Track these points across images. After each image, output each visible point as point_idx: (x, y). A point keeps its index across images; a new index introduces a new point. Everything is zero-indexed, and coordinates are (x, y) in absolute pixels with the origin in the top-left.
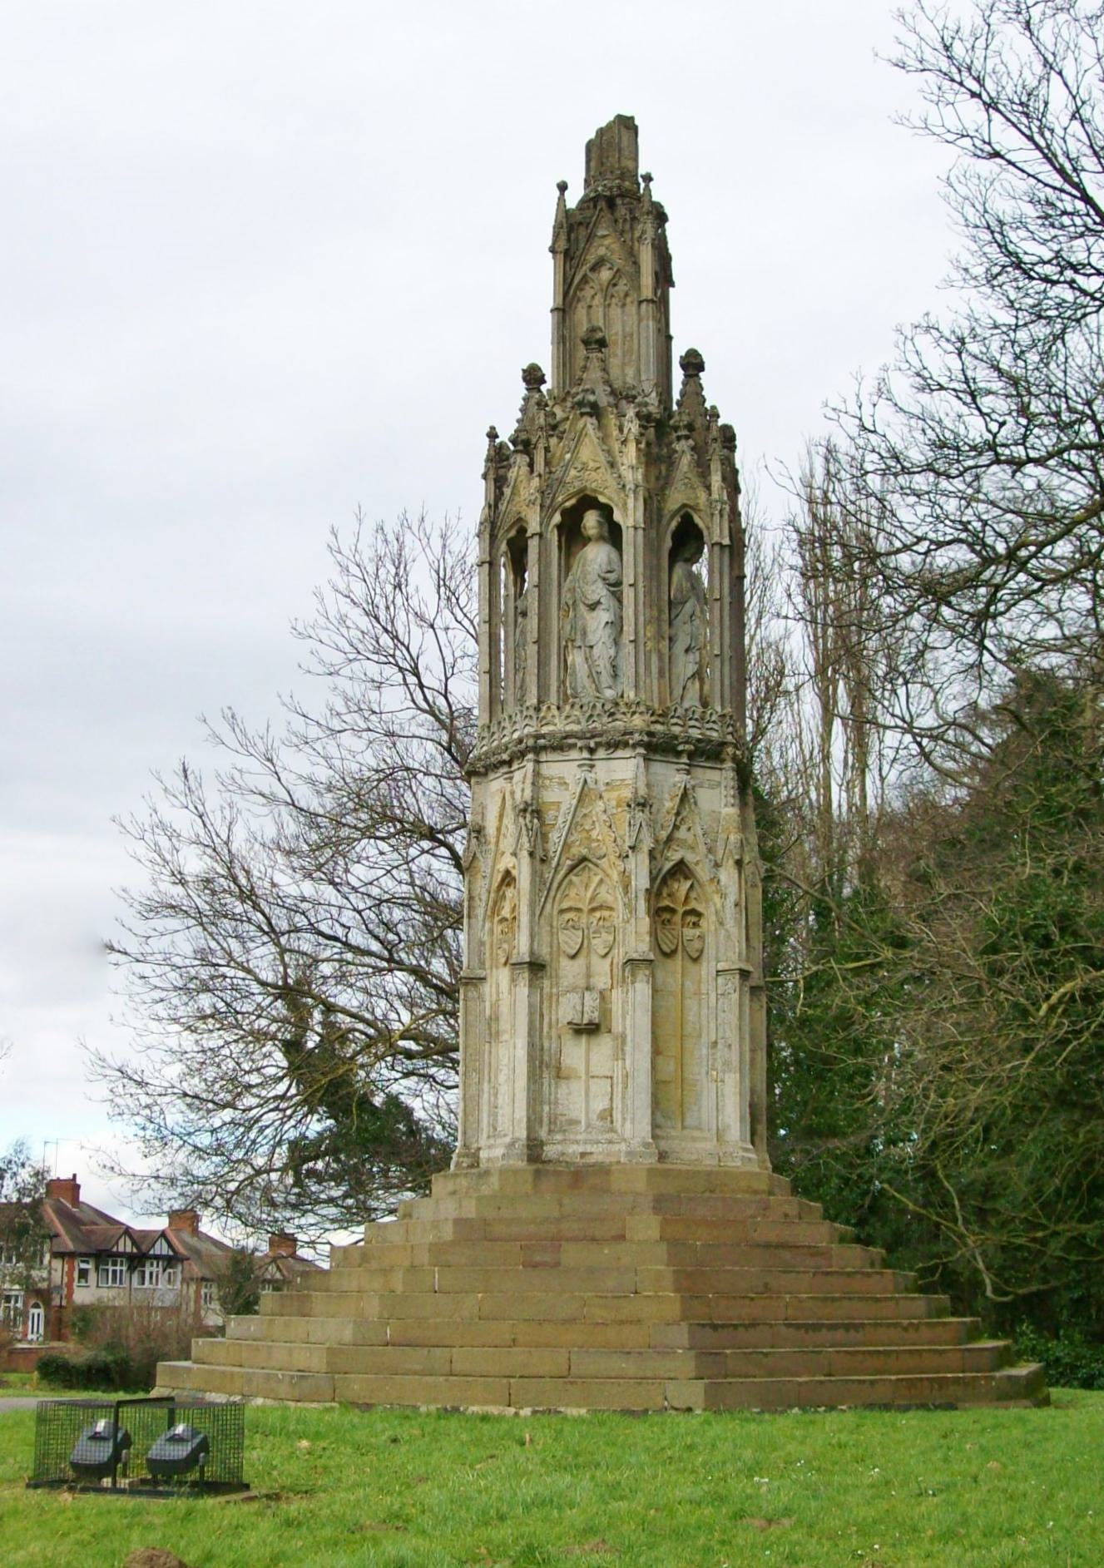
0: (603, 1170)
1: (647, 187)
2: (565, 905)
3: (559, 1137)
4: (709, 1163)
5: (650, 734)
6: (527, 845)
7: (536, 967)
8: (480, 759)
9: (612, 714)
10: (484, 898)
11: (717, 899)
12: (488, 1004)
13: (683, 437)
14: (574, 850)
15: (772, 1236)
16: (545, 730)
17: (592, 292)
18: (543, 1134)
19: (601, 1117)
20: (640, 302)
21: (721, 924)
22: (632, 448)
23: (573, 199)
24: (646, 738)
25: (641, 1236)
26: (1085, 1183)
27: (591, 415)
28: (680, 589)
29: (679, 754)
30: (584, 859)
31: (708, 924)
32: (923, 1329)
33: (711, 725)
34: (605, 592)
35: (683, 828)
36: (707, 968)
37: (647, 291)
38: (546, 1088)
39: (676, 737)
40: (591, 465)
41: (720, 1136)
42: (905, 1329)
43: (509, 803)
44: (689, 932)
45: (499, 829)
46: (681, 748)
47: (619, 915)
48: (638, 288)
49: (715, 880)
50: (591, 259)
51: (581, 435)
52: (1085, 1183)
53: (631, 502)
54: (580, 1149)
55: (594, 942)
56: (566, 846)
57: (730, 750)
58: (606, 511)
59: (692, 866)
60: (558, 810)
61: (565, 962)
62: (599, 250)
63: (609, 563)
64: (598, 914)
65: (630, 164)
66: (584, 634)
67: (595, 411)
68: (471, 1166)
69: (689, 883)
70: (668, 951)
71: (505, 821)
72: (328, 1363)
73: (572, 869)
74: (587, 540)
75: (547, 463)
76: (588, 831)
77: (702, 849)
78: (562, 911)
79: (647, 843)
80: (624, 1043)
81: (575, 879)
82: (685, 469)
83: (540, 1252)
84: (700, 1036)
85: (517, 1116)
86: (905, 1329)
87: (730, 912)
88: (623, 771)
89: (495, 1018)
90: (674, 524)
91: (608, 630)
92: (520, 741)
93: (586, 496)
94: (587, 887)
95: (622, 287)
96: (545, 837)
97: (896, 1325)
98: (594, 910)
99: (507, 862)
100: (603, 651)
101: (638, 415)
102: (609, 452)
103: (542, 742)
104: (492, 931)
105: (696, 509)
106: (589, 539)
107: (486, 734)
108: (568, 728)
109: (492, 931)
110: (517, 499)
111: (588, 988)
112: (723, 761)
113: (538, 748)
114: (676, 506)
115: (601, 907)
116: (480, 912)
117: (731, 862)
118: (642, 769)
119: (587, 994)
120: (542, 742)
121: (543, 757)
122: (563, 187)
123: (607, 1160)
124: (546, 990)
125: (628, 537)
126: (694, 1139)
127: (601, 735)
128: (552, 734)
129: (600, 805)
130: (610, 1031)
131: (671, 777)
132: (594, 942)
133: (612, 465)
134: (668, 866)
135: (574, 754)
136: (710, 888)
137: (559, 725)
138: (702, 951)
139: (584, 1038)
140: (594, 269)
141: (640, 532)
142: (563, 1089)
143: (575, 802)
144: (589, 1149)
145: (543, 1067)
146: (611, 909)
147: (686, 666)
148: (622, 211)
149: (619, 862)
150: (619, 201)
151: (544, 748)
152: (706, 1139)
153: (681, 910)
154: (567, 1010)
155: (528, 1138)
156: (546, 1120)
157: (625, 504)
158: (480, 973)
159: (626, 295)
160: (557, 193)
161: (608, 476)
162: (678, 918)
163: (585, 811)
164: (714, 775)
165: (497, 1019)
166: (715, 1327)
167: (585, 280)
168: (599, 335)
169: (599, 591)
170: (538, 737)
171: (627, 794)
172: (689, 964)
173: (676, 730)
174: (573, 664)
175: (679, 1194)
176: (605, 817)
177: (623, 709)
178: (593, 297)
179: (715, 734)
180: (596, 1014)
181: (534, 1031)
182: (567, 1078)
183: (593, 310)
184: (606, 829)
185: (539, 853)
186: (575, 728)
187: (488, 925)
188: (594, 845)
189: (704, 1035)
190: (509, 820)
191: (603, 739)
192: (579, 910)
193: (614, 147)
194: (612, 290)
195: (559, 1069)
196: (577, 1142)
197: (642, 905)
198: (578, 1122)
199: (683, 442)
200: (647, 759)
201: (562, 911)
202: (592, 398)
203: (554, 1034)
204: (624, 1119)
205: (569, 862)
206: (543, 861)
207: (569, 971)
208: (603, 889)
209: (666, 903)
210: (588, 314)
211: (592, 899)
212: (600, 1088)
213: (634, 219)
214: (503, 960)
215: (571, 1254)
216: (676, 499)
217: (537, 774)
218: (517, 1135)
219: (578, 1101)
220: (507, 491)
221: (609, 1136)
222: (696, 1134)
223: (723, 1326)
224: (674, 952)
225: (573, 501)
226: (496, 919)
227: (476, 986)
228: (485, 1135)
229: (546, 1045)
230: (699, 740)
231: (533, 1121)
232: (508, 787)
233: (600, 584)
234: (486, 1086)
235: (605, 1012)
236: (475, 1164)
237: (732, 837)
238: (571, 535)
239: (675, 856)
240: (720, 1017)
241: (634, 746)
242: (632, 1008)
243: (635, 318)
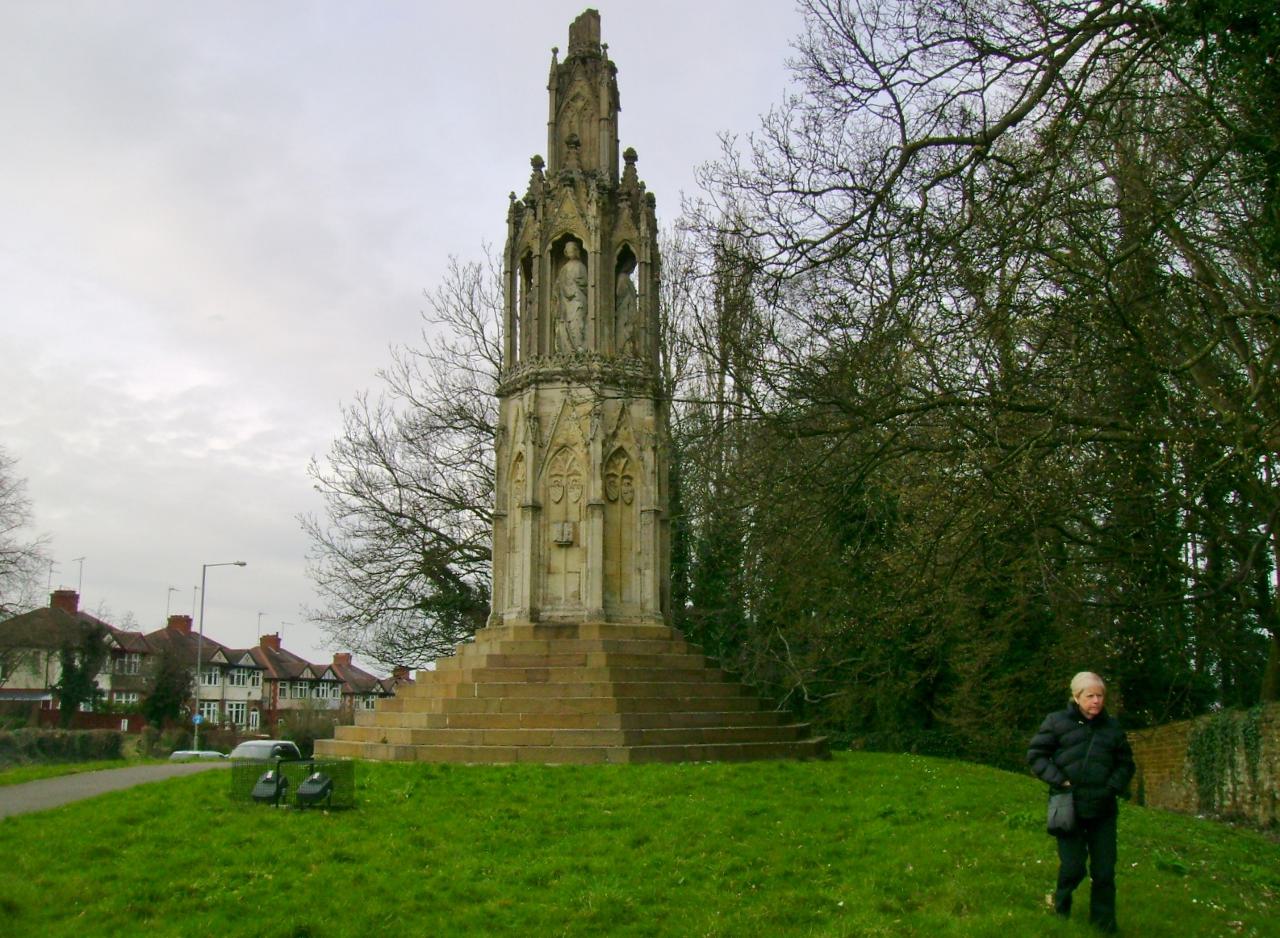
0: (574, 627)
2: (553, 473)
3: (549, 607)
16: (541, 370)
18: (540, 605)
19: (573, 596)
20: (600, 120)
36: (636, 509)
37: (604, 114)
40: (571, 215)
51: (566, 196)
54: (561, 614)
58: (579, 243)
64: (572, 478)
69: (624, 461)
78: (551, 476)
89: (512, 538)
90: (619, 250)
92: (527, 377)
94: (566, 462)
99: (519, 447)
102: (581, 208)
121: (541, 386)
122: (555, 51)
124: (542, 522)
125: (591, 257)
128: (546, 373)
133: (583, 216)
135: (559, 384)
139: (563, 550)
142: (552, 579)
144: (566, 614)
145: (541, 568)
148: (590, 66)
151: (542, 381)
154: (554, 533)
167: (568, 106)
168: (575, 139)
172: (625, 506)
193: (586, 28)
195: (549, 569)
197: (598, 473)
201: (551, 476)
207: (555, 512)
208: (575, 463)
217: (537, 396)
219: (560, 586)
224: (616, 500)
231: (534, 597)
233: (575, 285)
235: (576, 534)
238: (558, 256)
239: (617, 444)
242: (591, 533)
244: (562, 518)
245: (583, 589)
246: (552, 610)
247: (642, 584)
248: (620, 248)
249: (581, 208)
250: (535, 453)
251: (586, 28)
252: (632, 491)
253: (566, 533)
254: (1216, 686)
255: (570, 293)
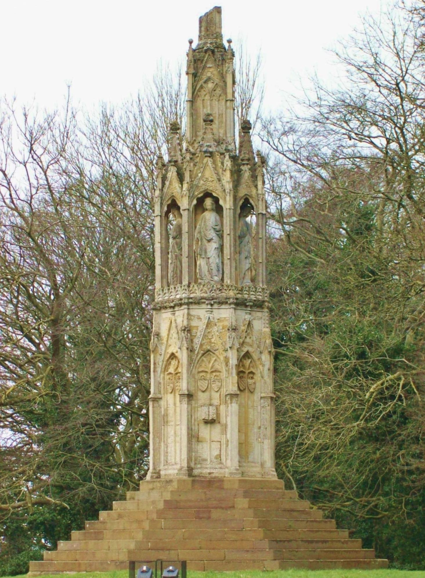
0: (221, 481)
1: (229, 46)
2: (200, 370)
3: (199, 466)
4: (259, 478)
5: (237, 299)
6: (186, 345)
7: (190, 396)
8: (158, 303)
9: (220, 290)
10: (161, 364)
11: (261, 367)
12: (163, 409)
13: (247, 164)
14: (204, 347)
15: (287, 506)
16: (192, 296)
17: (205, 93)
18: (192, 465)
19: (216, 458)
20: (227, 101)
21: (262, 377)
22: (228, 174)
23: (194, 46)
24: (235, 301)
25: (240, 506)
26: (380, 478)
27: (210, 157)
28: (242, 231)
29: (246, 306)
30: (209, 351)
31: (257, 377)
32: (349, 543)
33: (259, 293)
34: (214, 235)
35: (248, 337)
36: (256, 396)
38: (193, 446)
39: (246, 300)
40: (210, 179)
41: (262, 465)
42: (343, 543)
43: (174, 325)
44: (250, 381)
45: (168, 335)
46: (248, 304)
47: (224, 374)
48: (226, 94)
49: (260, 359)
50: (205, 78)
51: (206, 165)
52: (380, 478)
53: (228, 198)
54: (208, 471)
55: (213, 385)
56: (201, 345)
57: (266, 304)
58: (216, 200)
59: (251, 354)
60: (197, 329)
61: (200, 394)
62: (208, 73)
63: (216, 221)
64: (214, 374)
65: (218, 30)
66: (206, 252)
67: (211, 155)
68: (157, 478)
69: (250, 361)
70: (242, 389)
71: (172, 332)
72: (128, 557)
73: (203, 355)
74: (204, 210)
75: (191, 177)
76: (210, 339)
77: (255, 346)
78: (199, 372)
79: (237, 346)
80: (226, 427)
81: (205, 359)
82: (246, 178)
83: (202, 513)
84: (254, 424)
85: (183, 457)
86: (343, 543)
87: (266, 372)
88: (226, 314)
89: (166, 415)
90: (241, 203)
91: (216, 251)
92: (181, 299)
93: (207, 193)
94: (209, 362)
95: (218, 91)
96: (192, 341)
97: (339, 541)
98: (212, 372)
99: (173, 349)
100: (214, 260)
101: (230, 157)
102: (217, 174)
103: (191, 300)
104: (164, 378)
105: (252, 197)
106: (207, 210)
107: (161, 293)
108: (202, 295)
109: (164, 378)
110: (171, 187)
111: (210, 405)
112: (263, 308)
113: (191, 302)
114: (243, 195)
115: (215, 371)
116: (159, 370)
117: (266, 351)
118: (233, 314)
119: (211, 407)
120: (191, 300)
121: (191, 307)
122: (191, 42)
123: (220, 476)
124: (193, 405)
126: (252, 467)
127: (216, 299)
128: (195, 298)
129: (215, 329)
130: (219, 423)
131: (243, 315)
132: (213, 385)
133: (219, 180)
134: (243, 354)
135: (204, 306)
136: (258, 363)
137: (198, 294)
138: (254, 389)
139: (209, 425)
140: (206, 82)
141: (232, 211)
142: (200, 446)
143: (205, 327)
144: (212, 471)
145: (193, 438)
146: (220, 372)
147: (246, 264)
148: (218, 55)
149: (224, 353)
150: (216, 50)
151: (192, 303)
152: (256, 467)
153: (247, 372)
154: (203, 413)
155: (188, 467)
156: (193, 459)
157: (225, 198)
158: (159, 396)
159: (220, 96)
160: (189, 44)
161: (217, 185)
162: (246, 375)
163: (209, 330)
164: (259, 314)
165: (167, 415)
166: (277, 541)
167: (202, 87)
168: (211, 118)
169: (212, 234)
170: (189, 298)
171: (227, 324)
172: (250, 394)
173: (246, 296)
174: (200, 265)
175: (250, 488)
176: (218, 334)
177: (225, 288)
178: (205, 95)
179: (260, 297)
180: (215, 416)
181: (189, 421)
182: (201, 442)
183: (205, 101)
184: (218, 339)
185: (190, 348)
186: (205, 295)
187: (162, 375)
188: (213, 345)
189: (255, 423)
190: (174, 331)
191: (217, 301)
192: (206, 372)
193: (210, 23)
194: (214, 93)
195: (198, 438)
196: (207, 468)
197: (234, 372)
198: (206, 460)
199: (246, 166)
200: (235, 309)
201: (199, 372)
202: (211, 150)
203: (196, 424)
204: (226, 459)
205: (202, 352)
206: (191, 351)
207: (202, 397)
208: (216, 363)
209: (242, 369)
210: (203, 103)
211: (212, 367)
212: (215, 445)
213: (223, 60)
214: (170, 391)
215: (215, 514)
216: (243, 192)
217: (189, 314)
218: (183, 465)
219: (207, 451)
220: (167, 183)
221: (220, 466)
222: (253, 464)
223: (280, 541)
224: (245, 389)
225: (202, 195)
226: (166, 373)
227: (157, 401)
228: (162, 464)
229: (193, 428)
230: (255, 300)
231: (189, 459)
232: (173, 318)
233: (212, 231)
234: (162, 444)
235: (218, 414)
236: (159, 477)
237: (267, 341)
239: (245, 349)
240: (263, 415)
241: (230, 304)
242: (230, 414)
243: (224, 107)
244: (208, 402)
245: (223, 452)
246: (201, 468)
247: (262, 449)
248: (243, 201)
249: (217, 174)
250: (188, 356)
251: (210, 23)
252: (255, 383)
253: (211, 413)
254: (128, 322)
255: (210, 237)
